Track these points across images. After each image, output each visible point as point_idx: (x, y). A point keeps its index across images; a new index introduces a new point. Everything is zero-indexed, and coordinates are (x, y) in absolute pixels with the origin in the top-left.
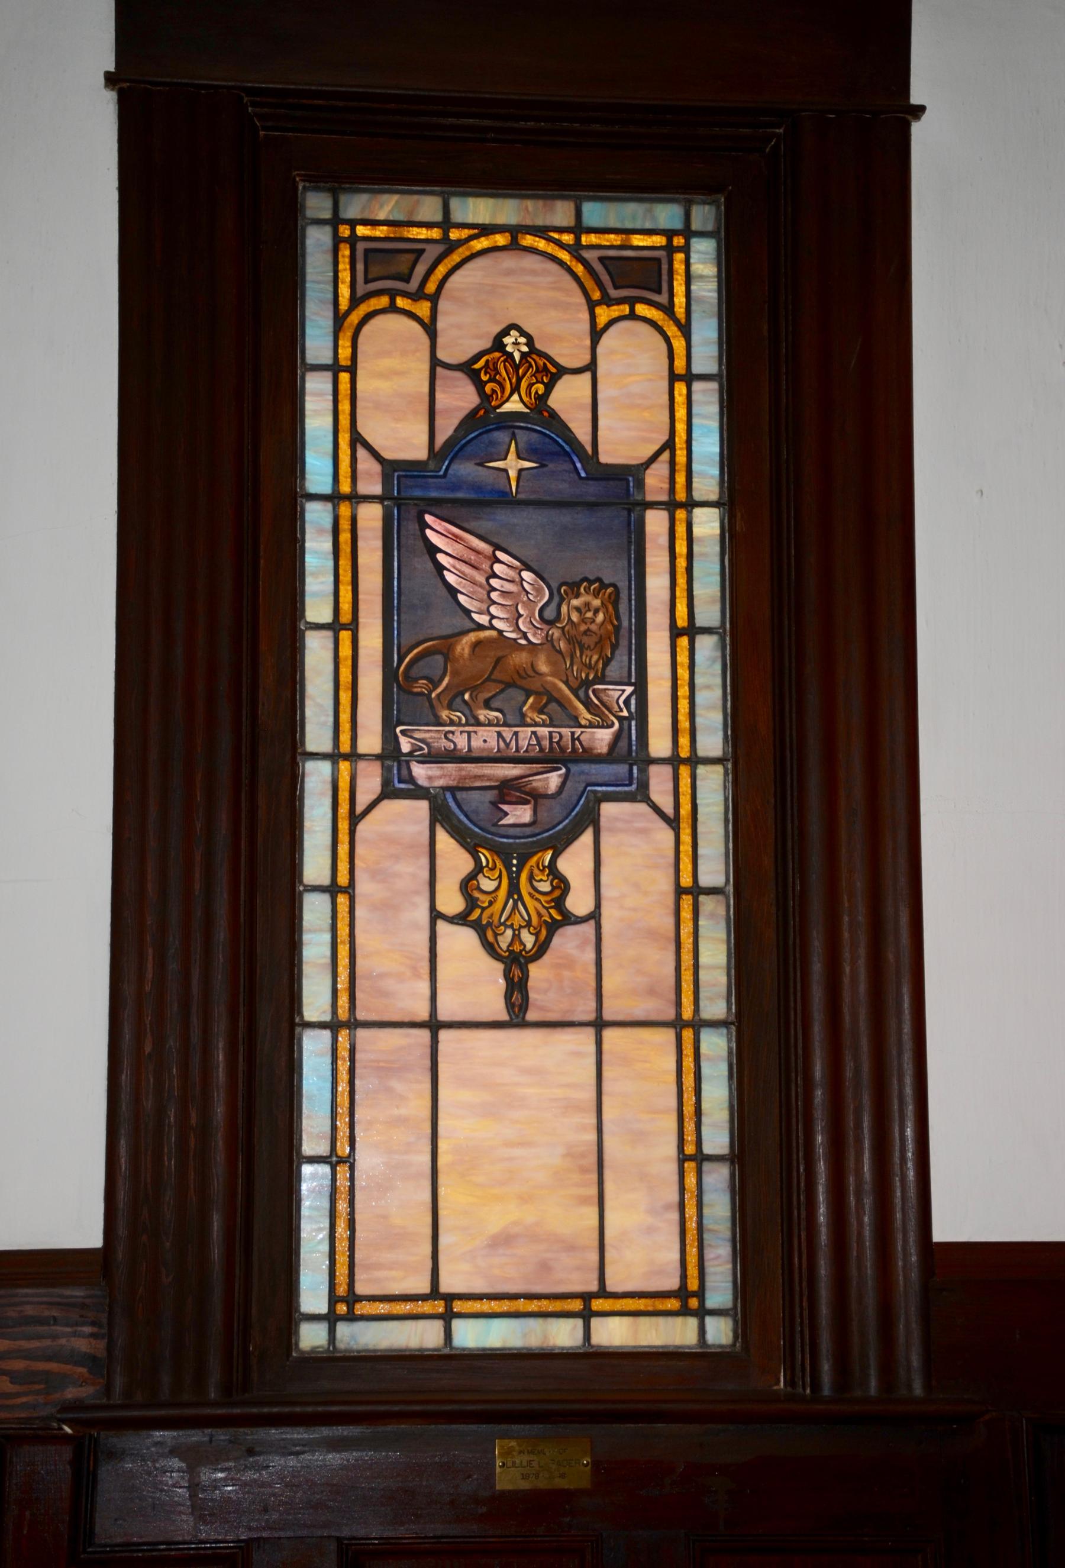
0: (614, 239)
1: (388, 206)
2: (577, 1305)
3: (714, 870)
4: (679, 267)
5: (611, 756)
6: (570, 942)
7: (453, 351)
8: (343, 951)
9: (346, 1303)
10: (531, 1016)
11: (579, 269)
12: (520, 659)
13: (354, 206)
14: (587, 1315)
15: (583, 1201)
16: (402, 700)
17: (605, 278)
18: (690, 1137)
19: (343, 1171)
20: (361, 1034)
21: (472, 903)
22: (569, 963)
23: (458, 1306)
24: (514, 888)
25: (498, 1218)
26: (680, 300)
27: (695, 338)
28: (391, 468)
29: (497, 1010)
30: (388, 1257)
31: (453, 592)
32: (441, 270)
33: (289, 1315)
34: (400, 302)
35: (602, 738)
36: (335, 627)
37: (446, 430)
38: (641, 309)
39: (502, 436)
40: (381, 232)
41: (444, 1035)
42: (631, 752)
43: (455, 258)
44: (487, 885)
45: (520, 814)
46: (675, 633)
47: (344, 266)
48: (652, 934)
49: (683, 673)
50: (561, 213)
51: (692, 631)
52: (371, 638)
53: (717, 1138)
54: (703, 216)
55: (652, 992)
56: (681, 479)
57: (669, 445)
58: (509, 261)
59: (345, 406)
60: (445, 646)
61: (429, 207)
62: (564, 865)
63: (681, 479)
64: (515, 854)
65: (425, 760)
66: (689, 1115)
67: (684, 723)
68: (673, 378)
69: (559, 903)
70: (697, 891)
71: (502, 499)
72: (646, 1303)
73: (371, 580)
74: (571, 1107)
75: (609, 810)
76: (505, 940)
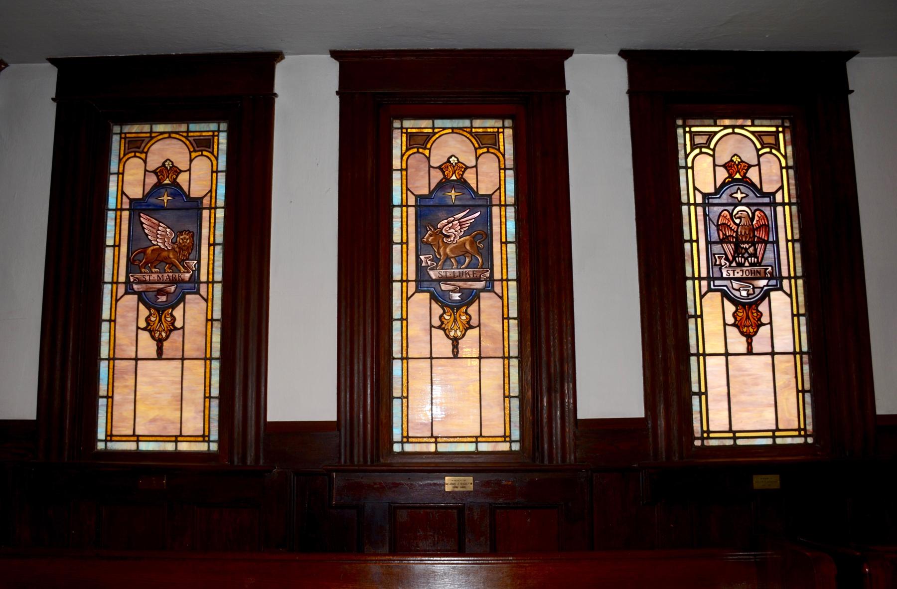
0: (198, 134)
1: (136, 128)
2: (174, 439)
3: (217, 315)
4: (216, 140)
6: (176, 336)
7: (435, 162)
9: (110, 437)
10: (164, 357)
11: (188, 143)
12: (165, 254)
13: (126, 129)
14: (176, 442)
15: (176, 410)
17: (195, 145)
18: (207, 391)
19: (110, 400)
20: (116, 362)
21: (148, 324)
22: (175, 341)
23: (140, 438)
24: (160, 320)
25: (152, 414)
26: (216, 150)
27: (219, 161)
28: (132, 201)
30: (121, 424)
31: (147, 235)
33: (94, 439)
34: (138, 154)
35: (187, 276)
38: (204, 153)
41: (139, 362)
42: (195, 280)
44: (153, 319)
46: (210, 245)
47: (123, 145)
48: (199, 333)
49: (211, 257)
50: (183, 127)
51: (214, 244)
52: (124, 249)
54: (224, 126)
55: (198, 349)
56: (213, 201)
57: (211, 191)
58: (168, 141)
59: (120, 184)
60: (144, 251)
61: (146, 128)
62: (174, 313)
63: (213, 201)
64: (161, 310)
66: (207, 385)
67: (211, 271)
69: (173, 324)
70: (212, 320)
71: (162, 208)
72: (193, 438)
73: (125, 233)
74: (174, 382)
75: (188, 297)
76: (157, 335)
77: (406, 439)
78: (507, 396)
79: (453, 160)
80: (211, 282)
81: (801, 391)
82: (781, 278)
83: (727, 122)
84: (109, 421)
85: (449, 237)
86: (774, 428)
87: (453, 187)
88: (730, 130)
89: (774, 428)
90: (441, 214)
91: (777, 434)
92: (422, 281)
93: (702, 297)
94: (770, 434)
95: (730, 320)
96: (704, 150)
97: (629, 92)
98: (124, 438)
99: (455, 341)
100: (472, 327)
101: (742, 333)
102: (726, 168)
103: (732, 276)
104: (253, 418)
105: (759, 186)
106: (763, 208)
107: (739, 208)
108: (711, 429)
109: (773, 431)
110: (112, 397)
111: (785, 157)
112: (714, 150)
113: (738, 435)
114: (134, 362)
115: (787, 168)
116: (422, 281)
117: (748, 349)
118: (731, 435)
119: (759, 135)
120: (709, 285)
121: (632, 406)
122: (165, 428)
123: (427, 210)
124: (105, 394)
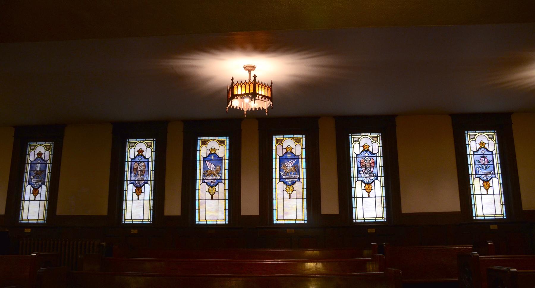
1: (204, 138)
6: (216, 194)
7: (208, 149)
13: (201, 138)
16: (204, 176)
25: (211, 214)
35: (219, 178)
45: (212, 184)
50: (217, 138)
64: (212, 187)
66: (225, 206)
71: (212, 160)
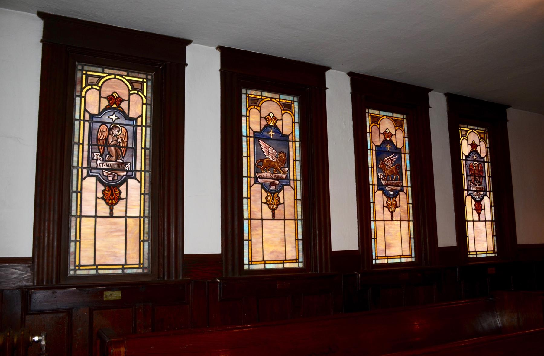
0: (284, 101)
1: (254, 92)
5: (285, 179)
6: (280, 207)
8: (249, 208)
9: (251, 262)
12: (273, 163)
14: (284, 263)
21: (267, 201)
22: (280, 210)
23: (266, 262)
24: (273, 199)
25: (272, 249)
29: (271, 217)
32: (261, 103)
35: (284, 176)
36: (247, 157)
37: (262, 127)
38: (288, 112)
39: (270, 129)
40: (253, 96)
42: (288, 178)
43: (263, 101)
44: (269, 198)
45: (273, 187)
46: (294, 161)
48: (291, 206)
50: (277, 96)
52: (375, 168)
53: (300, 237)
57: (292, 132)
58: (270, 102)
62: (279, 195)
64: (273, 193)
65: (260, 178)
68: (293, 122)
69: (279, 201)
70: (297, 200)
72: (291, 261)
73: (252, 150)
74: (281, 232)
75: (285, 187)
77: (377, 258)
78: (410, 238)
79: (115, 94)
80: (295, 180)
81: (493, 236)
82: (487, 191)
83: (472, 127)
84: (250, 253)
85: (388, 166)
86: (123, 262)
87: (388, 143)
88: (113, 76)
89: (123, 262)
90: (384, 155)
91: (125, 267)
92: (380, 186)
93: (82, 179)
94: (121, 267)
95: (100, 195)
96: (94, 87)
97: (507, 121)
98: (258, 262)
99: (392, 213)
100: (397, 207)
101: (107, 204)
102: (108, 99)
103: (101, 167)
104: (174, 255)
105: (127, 112)
106: (127, 127)
107: (475, 162)
108: (138, 263)
109: (123, 265)
110: (251, 240)
111: (146, 97)
112: (100, 87)
113: (99, 267)
114: (261, 221)
115: (146, 104)
116: (379, 185)
117: (110, 213)
118: (95, 267)
119: (131, 82)
120: (88, 172)
121: (453, 243)
122: (278, 256)
123: (380, 152)
124: (247, 238)
